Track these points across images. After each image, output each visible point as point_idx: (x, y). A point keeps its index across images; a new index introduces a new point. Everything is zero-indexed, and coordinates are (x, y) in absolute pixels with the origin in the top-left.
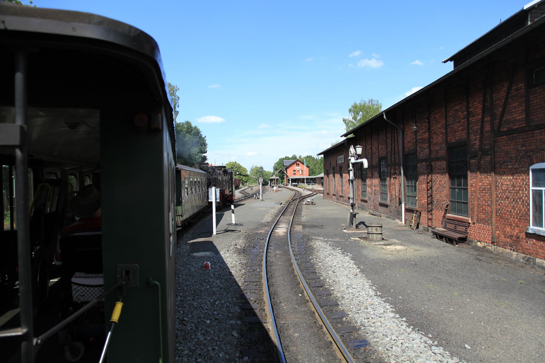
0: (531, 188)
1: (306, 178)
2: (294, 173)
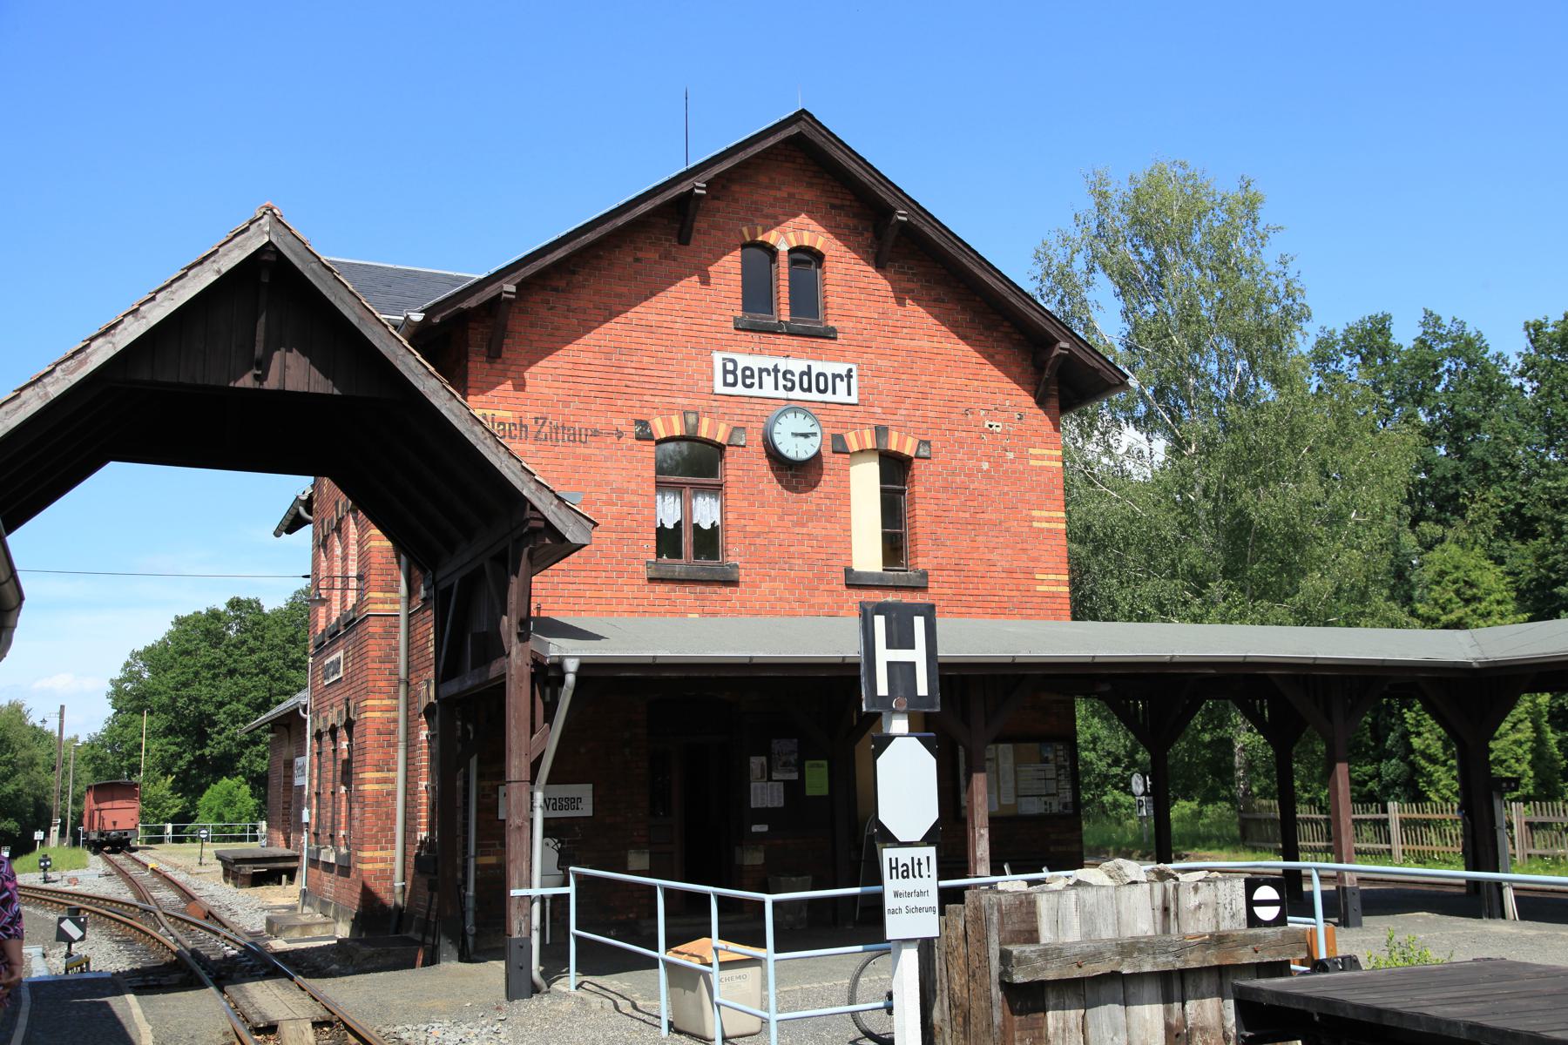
0: (769, 899)
1: (901, 534)
2: (668, 540)
